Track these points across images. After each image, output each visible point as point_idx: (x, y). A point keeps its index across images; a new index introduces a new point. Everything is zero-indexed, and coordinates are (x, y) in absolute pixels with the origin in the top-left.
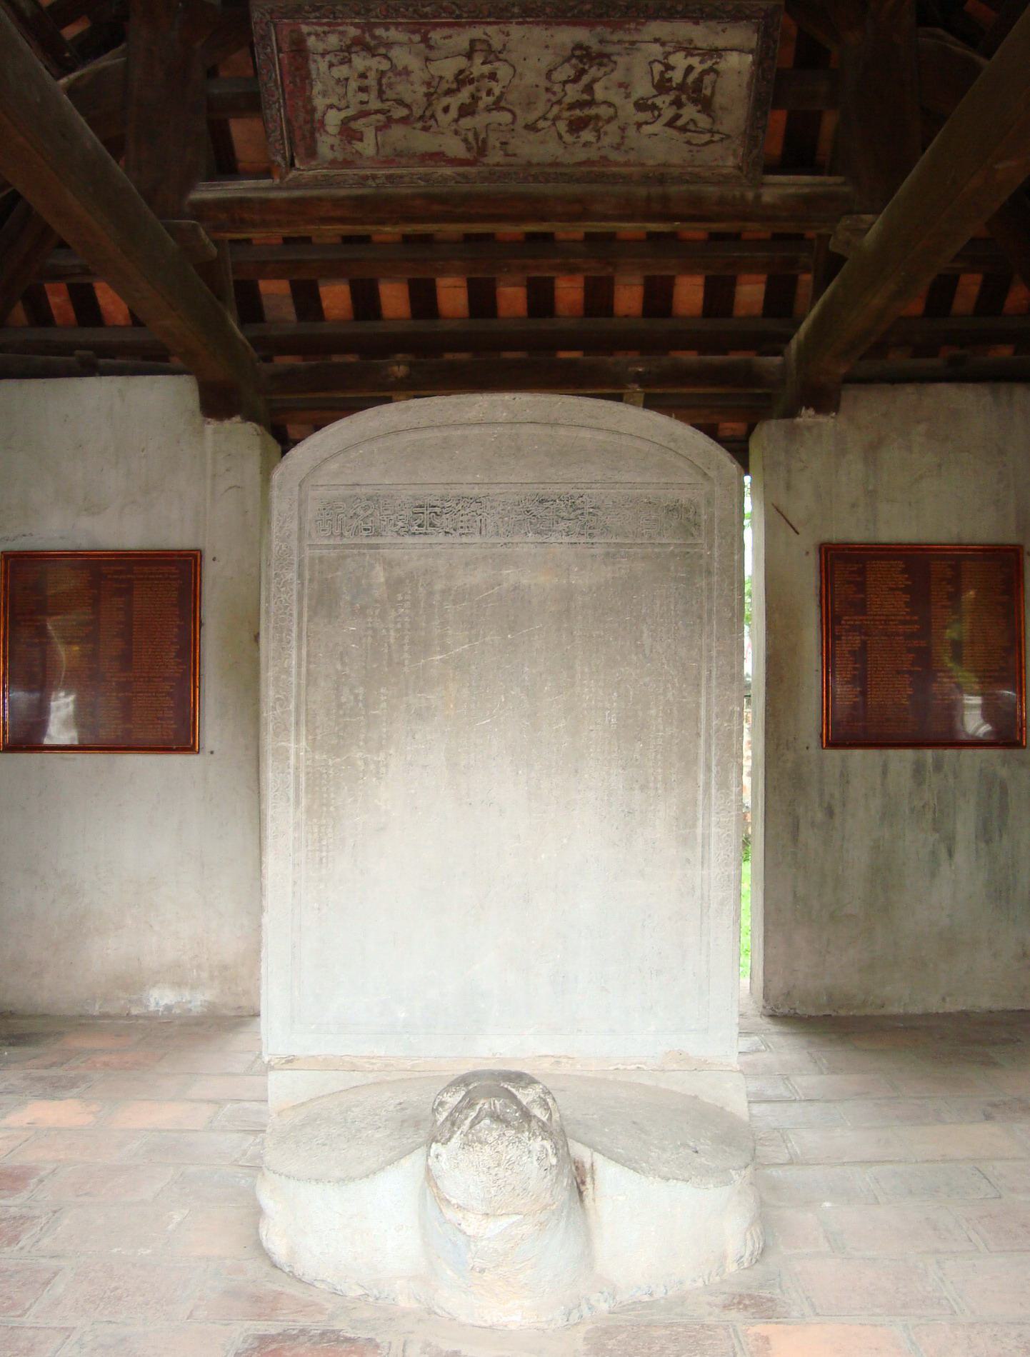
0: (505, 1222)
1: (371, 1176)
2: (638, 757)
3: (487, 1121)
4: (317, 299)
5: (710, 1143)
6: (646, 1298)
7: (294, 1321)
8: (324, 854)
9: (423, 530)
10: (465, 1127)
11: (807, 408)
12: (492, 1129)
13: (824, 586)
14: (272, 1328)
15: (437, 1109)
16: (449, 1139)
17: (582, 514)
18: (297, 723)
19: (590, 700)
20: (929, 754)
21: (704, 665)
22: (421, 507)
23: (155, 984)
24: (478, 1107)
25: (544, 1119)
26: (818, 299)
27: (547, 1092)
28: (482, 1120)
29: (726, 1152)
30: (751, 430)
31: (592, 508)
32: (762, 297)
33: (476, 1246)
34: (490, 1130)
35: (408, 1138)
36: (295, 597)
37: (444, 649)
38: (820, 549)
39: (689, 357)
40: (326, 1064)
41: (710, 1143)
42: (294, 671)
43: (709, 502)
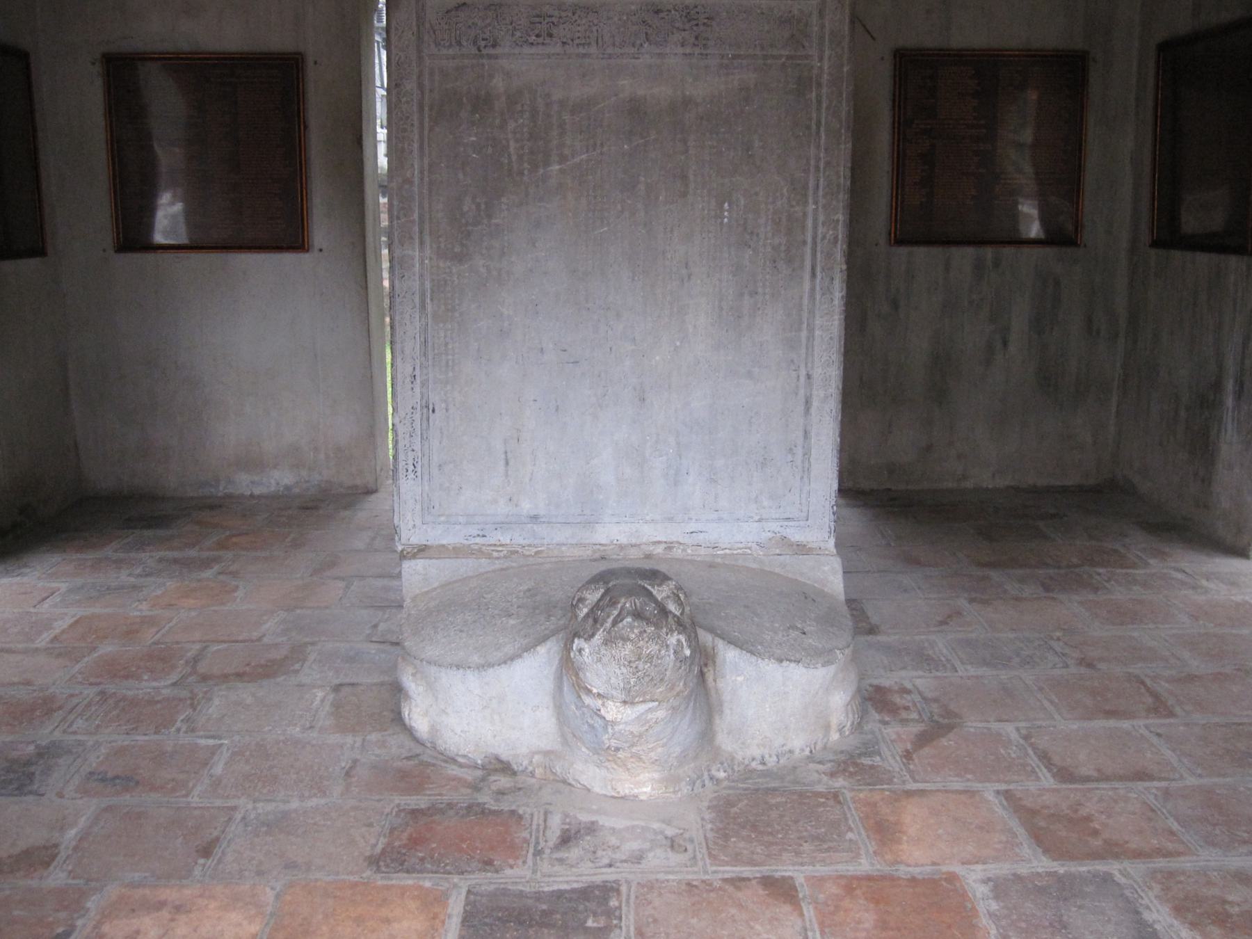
0: (641, 708)
1: (509, 662)
2: (748, 264)
3: (629, 619)
6: (760, 767)
8: (450, 357)
9: (540, 40)
10: (608, 624)
12: (634, 627)
14: (420, 801)
16: (593, 635)
17: (697, 25)
18: (421, 232)
20: (989, 252)
22: (538, 16)
23: (275, 467)
24: (619, 606)
25: (678, 613)
27: (679, 588)
31: (708, 18)
33: (612, 729)
34: (632, 628)
36: (415, 108)
37: (563, 159)
38: (895, 57)
40: (458, 552)
41: (815, 624)
42: (416, 181)
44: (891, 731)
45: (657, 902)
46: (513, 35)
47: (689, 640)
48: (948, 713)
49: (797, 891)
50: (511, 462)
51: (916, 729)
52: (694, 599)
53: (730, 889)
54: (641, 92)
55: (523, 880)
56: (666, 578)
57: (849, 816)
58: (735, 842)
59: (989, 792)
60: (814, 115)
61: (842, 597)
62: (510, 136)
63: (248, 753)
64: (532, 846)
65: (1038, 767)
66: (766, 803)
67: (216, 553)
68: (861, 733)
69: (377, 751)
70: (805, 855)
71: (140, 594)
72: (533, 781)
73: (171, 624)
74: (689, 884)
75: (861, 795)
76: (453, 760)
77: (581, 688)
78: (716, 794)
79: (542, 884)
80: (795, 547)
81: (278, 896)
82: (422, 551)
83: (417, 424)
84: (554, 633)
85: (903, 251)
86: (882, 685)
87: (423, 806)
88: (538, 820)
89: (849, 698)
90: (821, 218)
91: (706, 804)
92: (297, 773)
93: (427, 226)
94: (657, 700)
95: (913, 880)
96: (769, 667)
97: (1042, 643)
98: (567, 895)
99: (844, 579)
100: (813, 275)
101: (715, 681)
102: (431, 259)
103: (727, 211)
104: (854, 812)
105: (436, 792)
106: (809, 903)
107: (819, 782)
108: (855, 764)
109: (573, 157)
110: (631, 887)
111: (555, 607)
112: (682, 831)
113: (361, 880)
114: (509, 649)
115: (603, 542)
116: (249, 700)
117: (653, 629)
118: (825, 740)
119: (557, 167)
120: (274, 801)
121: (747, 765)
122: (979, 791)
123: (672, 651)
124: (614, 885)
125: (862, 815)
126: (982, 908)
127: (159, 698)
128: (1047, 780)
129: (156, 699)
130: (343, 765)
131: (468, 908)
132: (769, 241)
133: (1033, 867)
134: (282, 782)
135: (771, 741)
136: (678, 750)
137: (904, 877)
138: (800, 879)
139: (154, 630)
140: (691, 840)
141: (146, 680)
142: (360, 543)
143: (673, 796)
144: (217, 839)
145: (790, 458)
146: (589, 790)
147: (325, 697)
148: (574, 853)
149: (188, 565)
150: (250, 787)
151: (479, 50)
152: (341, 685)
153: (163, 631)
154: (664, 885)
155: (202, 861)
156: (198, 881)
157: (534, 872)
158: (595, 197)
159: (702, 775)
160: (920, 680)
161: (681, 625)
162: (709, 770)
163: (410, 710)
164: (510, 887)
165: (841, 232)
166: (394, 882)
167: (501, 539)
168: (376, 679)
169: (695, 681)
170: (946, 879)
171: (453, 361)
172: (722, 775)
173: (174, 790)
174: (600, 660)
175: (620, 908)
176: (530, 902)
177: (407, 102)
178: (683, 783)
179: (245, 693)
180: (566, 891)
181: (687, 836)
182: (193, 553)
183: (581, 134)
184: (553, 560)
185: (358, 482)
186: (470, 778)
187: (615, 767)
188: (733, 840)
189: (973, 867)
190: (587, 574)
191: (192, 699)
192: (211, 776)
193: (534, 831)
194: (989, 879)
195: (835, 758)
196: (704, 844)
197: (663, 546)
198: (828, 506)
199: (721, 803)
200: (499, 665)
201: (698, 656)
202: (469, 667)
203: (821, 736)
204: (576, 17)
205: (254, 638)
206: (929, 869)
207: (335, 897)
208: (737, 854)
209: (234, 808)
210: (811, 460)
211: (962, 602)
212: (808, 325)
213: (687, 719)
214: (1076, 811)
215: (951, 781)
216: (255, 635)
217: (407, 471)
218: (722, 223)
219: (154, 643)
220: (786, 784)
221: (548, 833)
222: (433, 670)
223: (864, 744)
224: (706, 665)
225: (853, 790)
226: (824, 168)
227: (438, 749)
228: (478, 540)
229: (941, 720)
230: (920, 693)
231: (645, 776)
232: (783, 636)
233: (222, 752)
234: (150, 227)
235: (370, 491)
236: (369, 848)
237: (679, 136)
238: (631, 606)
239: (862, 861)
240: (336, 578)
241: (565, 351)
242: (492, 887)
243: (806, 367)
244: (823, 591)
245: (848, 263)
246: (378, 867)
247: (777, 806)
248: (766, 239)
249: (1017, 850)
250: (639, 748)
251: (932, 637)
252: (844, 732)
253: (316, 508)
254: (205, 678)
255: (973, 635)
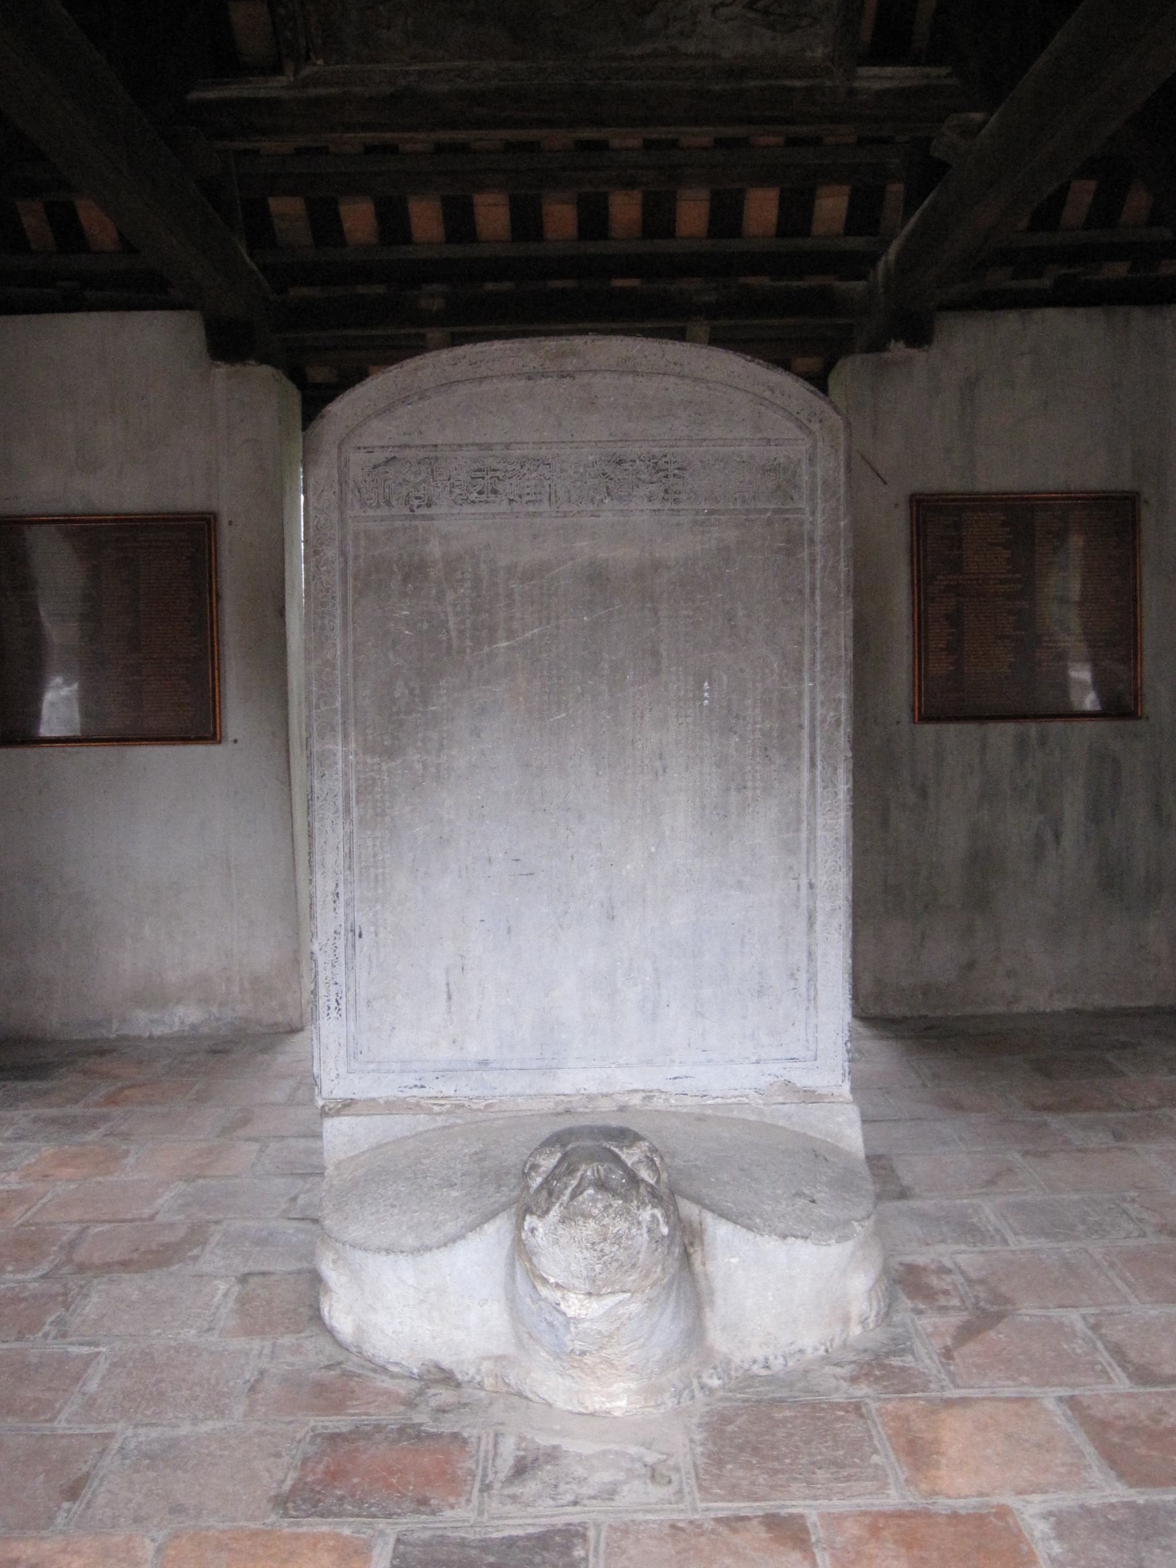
0: (610, 1301)
3: (591, 1191)
4: (336, 219)
5: (826, 1189)
6: (764, 1372)
7: (366, 1414)
8: (380, 871)
9: (483, 497)
10: (565, 1198)
11: (897, 340)
13: (915, 543)
14: (339, 1423)
15: (529, 1173)
16: (547, 1211)
17: (666, 477)
18: (344, 723)
19: (678, 689)
20: (1033, 729)
21: (807, 648)
22: (480, 470)
23: (179, 1001)
24: (579, 1174)
25: (652, 1182)
26: (912, 215)
27: (654, 1150)
28: (585, 1190)
29: (845, 1199)
30: (830, 365)
31: (678, 469)
32: (844, 213)
33: (576, 1328)
34: (594, 1201)
35: (490, 1197)
36: (337, 578)
37: (511, 635)
38: (911, 501)
39: (760, 282)
40: (391, 1107)
42: (339, 663)
43: (810, 460)
44: (927, 1323)
45: (632, 1552)
46: (451, 492)
47: (667, 1216)
48: (998, 1298)
49: (808, 1533)
50: (455, 997)
51: (955, 1319)
52: (679, 1162)
53: (724, 1531)
54: (602, 555)
55: (466, 1524)
56: (637, 1138)
57: (874, 1432)
58: (731, 1471)
59: (1049, 1398)
60: (808, 578)
61: (861, 1155)
62: (449, 609)
63: (130, 1364)
64: (478, 1479)
65: (1110, 1365)
66: (771, 1418)
67: (105, 1110)
68: (889, 1325)
69: (290, 1359)
70: (819, 1486)
71: (9, 1162)
72: (483, 1394)
73: (44, 1201)
74: (673, 1526)
75: (890, 1407)
76: (384, 1370)
77: (536, 1277)
78: (708, 1408)
79: (490, 1529)
80: (802, 1094)
81: (159, 1550)
82: (347, 1106)
83: (341, 951)
84: (504, 1208)
85: (929, 729)
86: (916, 1263)
87: (344, 1430)
88: (486, 1444)
89: (871, 1283)
90: (820, 697)
91: (695, 1420)
92: (190, 1389)
93: (351, 715)
94: (629, 1291)
95: (954, 1517)
96: (770, 1244)
97: (1113, 1206)
98: (520, 1543)
99: (863, 1130)
100: (813, 764)
101: (704, 1264)
102: (356, 754)
103: (707, 691)
104: (880, 1428)
105: (362, 1409)
106: (825, 1549)
107: (837, 1389)
108: (882, 1366)
109: (524, 632)
110: (600, 1531)
111: (507, 1174)
112: (665, 1457)
113: (263, 1527)
114: (451, 1228)
115: (567, 1092)
116: (135, 1296)
117: (620, 1202)
118: (844, 1335)
119: (506, 644)
120: (160, 1425)
121: (747, 1370)
122: (1036, 1398)
123: (645, 1230)
124: (579, 1528)
125: (890, 1432)
126: (1040, 1550)
127: (26, 1294)
128: (1122, 1383)
129: (22, 1296)
130: (247, 1377)
131: (396, 1562)
132: (758, 726)
133: (1106, 1496)
134: (171, 1400)
135: (776, 1338)
136: (658, 1353)
137: (944, 1512)
138: (812, 1517)
139: (22, 1208)
140: (677, 1469)
141: (10, 1272)
142: (278, 1095)
143: (655, 1411)
144: (88, 1474)
145: (792, 984)
146: (550, 1405)
147: (229, 1290)
148: (530, 1487)
149: (69, 1125)
150: (131, 1408)
151: (412, 511)
152: (250, 1274)
153: (34, 1210)
154: (642, 1528)
155: (66, 1505)
156: (61, 1532)
157: (481, 1513)
158: (550, 678)
159: (691, 1383)
160: (964, 1256)
161: (655, 1196)
162: (699, 1377)
163: (331, 1306)
164: (449, 1534)
165: (844, 714)
166: (304, 1529)
167: (444, 1089)
168: (294, 1266)
169: (677, 1265)
170: (996, 1514)
171: (383, 873)
172: (715, 1382)
173: (36, 1413)
174: (556, 1242)
175: (586, 1559)
176: (473, 1552)
177: (328, 572)
178: (667, 1395)
179: (131, 1286)
180: (519, 1538)
181: (671, 1462)
182: (76, 1110)
183: (532, 605)
184: (507, 1114)
185: (280, 1018)
186: (403, 1392)
187: (581, 1375)
188: (730, 1466)
189: (1027, 1497)
190: (546, 1132)
191: (65, 1294)
192: (84, 1394)
193: (481, 1461)
194: (1051, 1514)
195: (855, 1358)
196: (693, 1475)
197: (641, 1095)
198: (840, 1042)
199: (716, 1418)
200: (438, 1248)
201: (679, 1233)
202: (402, 1252)
203: (838, 1330)
204: (525, 471)
205: (145, 1216)
206: (974, 1501)
207: (230, 1550)
208: (734, 1486)
209: (109, 1436)
210: (819, 987)
211: (1014, 1156)
212: (809, 824)
213: (670, 1310)
214: (1157, 1422)
215: (1003, 1386)
216: (147, 1212)
217: (329, 1008)
218: (701, 705)
219: (22, 1225)
220: (797, 1394)
221: (499, 1462)
222: (359, 1255)
223: (894, 1339)
224: (692, 1244)
225: (880, 1399)
226: (821, 639)
227: (365, 1354)
228: (415, 1092)
229: (988, 1306)
230: (963, 1273)
231: (618, 1386)
232: (788, 1206)
233: (98, 1364)
234: (36, 716)
235: (294, 1030)
236: (274, 1485)
237: (649, 605)
238: (593, 1174)
239: (890, 1492)
240: (248, 1139)
241: (517, 860)
242: (427, 1535)
243: (808, 875)
244: (838, 1147)
245: (853, 749)
246: (286, 1509)
247: (784, 1421)
248: (755, 723)
249: (1084, 1474)
250: (610, 1351)
251: (976, 1201)
252: (868, 1324)
253: (226, 1052)
254: (82, 1268)
255: (1028, 1198)
